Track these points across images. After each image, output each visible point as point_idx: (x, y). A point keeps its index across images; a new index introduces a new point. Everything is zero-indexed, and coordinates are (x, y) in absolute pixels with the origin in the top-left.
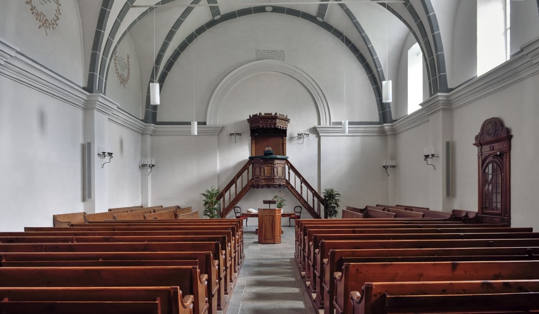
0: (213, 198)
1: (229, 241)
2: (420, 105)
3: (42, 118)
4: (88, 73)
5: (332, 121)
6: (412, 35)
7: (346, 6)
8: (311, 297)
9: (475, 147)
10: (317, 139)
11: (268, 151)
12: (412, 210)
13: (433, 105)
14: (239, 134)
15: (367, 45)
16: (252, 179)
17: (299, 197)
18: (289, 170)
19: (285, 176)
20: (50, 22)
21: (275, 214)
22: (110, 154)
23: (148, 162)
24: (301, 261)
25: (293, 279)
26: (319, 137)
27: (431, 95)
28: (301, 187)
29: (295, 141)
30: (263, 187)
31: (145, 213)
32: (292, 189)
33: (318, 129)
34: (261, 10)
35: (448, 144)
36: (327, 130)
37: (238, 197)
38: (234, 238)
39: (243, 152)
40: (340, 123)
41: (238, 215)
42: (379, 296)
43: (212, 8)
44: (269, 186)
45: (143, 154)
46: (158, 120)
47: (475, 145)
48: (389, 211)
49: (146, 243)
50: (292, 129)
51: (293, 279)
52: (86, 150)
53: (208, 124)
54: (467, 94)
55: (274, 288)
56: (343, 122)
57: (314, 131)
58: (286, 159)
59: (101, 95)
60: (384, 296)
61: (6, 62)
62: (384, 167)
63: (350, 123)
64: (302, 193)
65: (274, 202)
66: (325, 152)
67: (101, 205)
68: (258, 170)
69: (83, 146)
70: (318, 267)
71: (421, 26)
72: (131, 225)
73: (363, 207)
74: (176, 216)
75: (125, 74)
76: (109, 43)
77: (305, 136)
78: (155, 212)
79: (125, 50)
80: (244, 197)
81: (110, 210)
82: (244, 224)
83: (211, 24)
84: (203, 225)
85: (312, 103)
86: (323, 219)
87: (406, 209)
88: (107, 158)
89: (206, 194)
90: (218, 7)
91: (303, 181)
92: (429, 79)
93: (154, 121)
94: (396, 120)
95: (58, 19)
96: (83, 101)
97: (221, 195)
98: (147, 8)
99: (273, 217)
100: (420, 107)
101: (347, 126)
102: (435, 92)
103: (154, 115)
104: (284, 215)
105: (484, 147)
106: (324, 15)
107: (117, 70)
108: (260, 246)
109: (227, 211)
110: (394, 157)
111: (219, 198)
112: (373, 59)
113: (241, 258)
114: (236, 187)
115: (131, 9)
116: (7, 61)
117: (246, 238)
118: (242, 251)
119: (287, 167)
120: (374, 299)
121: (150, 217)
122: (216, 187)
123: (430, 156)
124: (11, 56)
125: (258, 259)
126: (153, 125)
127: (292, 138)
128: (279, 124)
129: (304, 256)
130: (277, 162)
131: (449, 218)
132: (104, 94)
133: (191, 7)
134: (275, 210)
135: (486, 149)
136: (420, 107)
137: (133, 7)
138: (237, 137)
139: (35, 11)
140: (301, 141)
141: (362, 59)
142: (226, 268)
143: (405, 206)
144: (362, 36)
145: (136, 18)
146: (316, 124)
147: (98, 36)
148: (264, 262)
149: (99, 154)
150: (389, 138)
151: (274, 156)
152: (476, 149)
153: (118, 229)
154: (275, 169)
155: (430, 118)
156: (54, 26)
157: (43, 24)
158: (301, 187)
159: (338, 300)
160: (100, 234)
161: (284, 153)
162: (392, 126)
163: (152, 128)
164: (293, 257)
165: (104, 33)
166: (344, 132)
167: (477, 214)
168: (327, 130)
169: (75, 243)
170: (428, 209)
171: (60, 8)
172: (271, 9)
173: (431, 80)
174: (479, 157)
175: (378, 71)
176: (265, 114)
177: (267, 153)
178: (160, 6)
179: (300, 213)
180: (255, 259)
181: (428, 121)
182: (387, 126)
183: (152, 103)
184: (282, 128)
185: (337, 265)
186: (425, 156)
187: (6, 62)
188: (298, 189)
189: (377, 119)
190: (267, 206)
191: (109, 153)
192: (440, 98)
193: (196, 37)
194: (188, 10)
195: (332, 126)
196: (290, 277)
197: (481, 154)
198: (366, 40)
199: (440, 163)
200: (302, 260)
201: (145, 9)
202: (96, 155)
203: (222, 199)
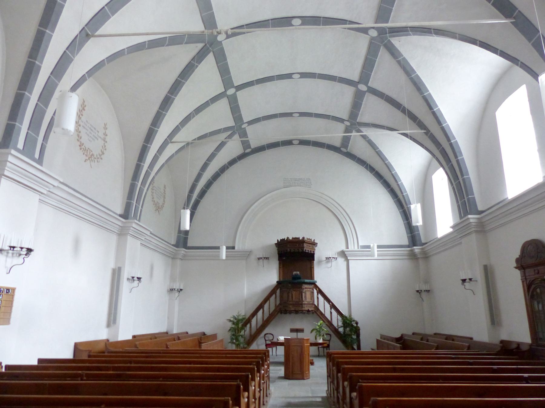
0: (239, 324)
1: (253, 379)
3: (77, 244)
4: (125, 201)
5: (360, 244)
7: (368, 138)
9: (517, 270)
10: (345, 263)
11: (296, 275)
12: (453, 340)
16: (280, 304)
17: (329, 324)
18: (318, 294)
19: (314, 301)
20: (95, 156)
22: (139, 279)
23: (176, 286)
24: (334, 402)
26: (347, 261)
27: (461, 218)
28: (331, 313)
29: (324, 265)
30: (290, 312)
31: (169, 340)
32: (322, 316)
33: (346, 253)
34: (288, 143)
36: (355, 254)
37: (266, 323)
38: (258, 374)
39: (271, 276)
40: (369, 247)
43: (243, 143)
44: (297, 312)
45: (173, 279)
46: (189, 244)
47: (516, 268)
48: (427, 341)
50: (320, 253)
52: (116, 274)
53: (236, 248)
56: (372, 245)
57: (343, 254)
58: (314, 284)
59: (136, 221)
61: (49, 191)
62: (418, 291)
63: (379, 247)
64: (331, 319)
66: (356, 276)
67: (125, 333)
68: (285, 295)
69: (114, 271)
72: (150, 357)
73: (398, 335)
75: (161, 202)
76: (147, 174)
77: (333, 260)
78: (179, 339)
82: (270, 353)
83: (242, 157)
85: (339, 227)
87: (446, 339)
88: (136, 282)
89: (232, 319)
90: (248, 141)
91: (333, 306)
92: (457, 202)
93: (185, 246)
94: (426, 243)
95: (103, 153)
96: (118, 226)
97: (248, 321)
98: (185, 144)
99: (302, 347)
100: (451, 230)
101: (376, 249)
102: (465, 215)
103: (185, 240)
105: (527, 270)
106: (348, 146)
107: (153, 198)
108: (287, 382)
109: (253, 338)
110: (426, 282)
111: (245, 325)
112: (398, 185)
113: (267, 396)
115: (170, 144)
116: (51, 190)
117: (273, 370)
118: (268, 388)
119: (315, 291)
121: (173, 346)
122: (244, 312)
123: (468, 280)
124: (54, 186)
125: (286, 398)
126: (184, 249)
127: (320, 262)
128: (307, 248)
129: (338, 398)
130: (305, 286)
131: (499, 351)
132: (139, 221)
135: (530, 272)
136: (451, 230)
137: (171, 142)
138: (265, 261)
139: (83, 147)
140: (329, 265)
142: (255, 399)
144: (386, 164)
145: (174, 152)
146: (343, 248)
147: (138, 168)
149: (128, 279)
150: (421, 262)
151: (302, 280)
152: (518, 274)
154: (303, 294)
156: (99, 160)
157: (89, 158)
158: (331, 313)
161: (312, 277)
162: (422, 249)
163: (183, 252)
165: (143, 166)
166: (374, 256)
167: (531, 345)
168: (355, 254)
170: (471, 339)
171: (106, 144)
172: (298, 142)
174: (523, 282)
175: (403, 196)
177: (296, 278)
178: (197, 141)
179: (329, 341)
180: (282, 397)
181: (461, 243)
182: (417, 249)
183: (182, 229)
184: (310, 252)
186: (462, 280)
187: (49, 191)
188: (328, 315)
189: (406, 242)
191: (138, 278)
192: (471, 221)
193: (228, 168)
194: (222, 145)
195: (360, 249)
197: (524, 278)
198: (389, 167)
199: (480, 287)
200: (336, 400)
201: (183, 144)
202: (125, 280)
203: (248, 326)
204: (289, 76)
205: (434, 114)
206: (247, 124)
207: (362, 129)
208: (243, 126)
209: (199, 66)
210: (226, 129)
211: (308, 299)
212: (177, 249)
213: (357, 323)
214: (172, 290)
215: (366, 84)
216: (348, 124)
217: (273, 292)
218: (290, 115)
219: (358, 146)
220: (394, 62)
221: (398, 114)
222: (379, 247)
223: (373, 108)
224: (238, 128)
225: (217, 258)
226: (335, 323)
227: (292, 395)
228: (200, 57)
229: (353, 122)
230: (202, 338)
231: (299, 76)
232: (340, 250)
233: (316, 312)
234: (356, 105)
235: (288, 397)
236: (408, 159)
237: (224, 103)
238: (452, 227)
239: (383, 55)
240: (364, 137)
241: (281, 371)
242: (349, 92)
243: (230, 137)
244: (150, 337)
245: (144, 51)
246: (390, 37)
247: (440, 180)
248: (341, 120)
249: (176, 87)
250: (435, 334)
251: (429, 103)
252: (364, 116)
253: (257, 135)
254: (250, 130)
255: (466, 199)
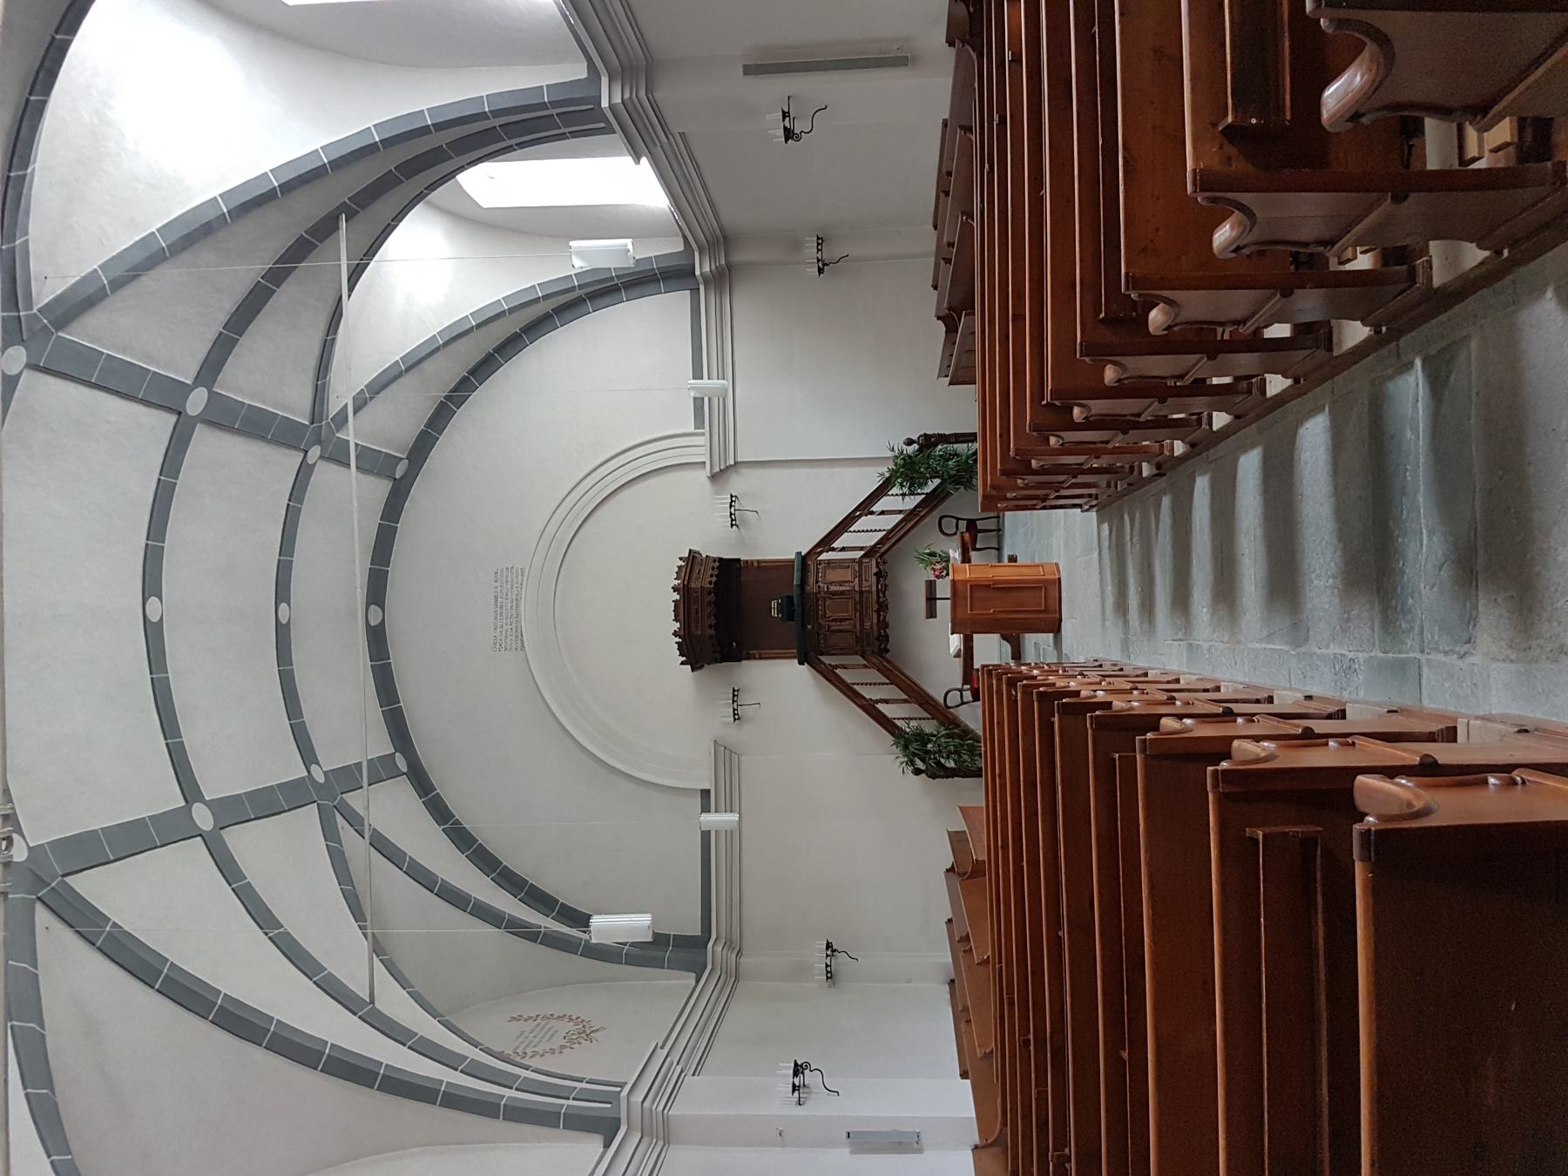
2: (637, 161)
4: (560, 1132)
5: (691, 429)
6: (434, 195)
8: (1226, 432)
10: (745, 471)
13: (636, 118)
14: (735, 694)
15: (471, 330)
17: (912, 518)
18: (834, 549)
21: (966, 581)
22: (798, 1070)
23: (819, 960)
25: (1166, 501)
28: (883, 513)
30: (884, 625)
32: (892, 539)
34: (377, 639)
35: (749, 70)
39: (783, 684)
40: (699, 403)
41: (968, 696)
42: (1232, 150)
44: (883, 607)
48: (949, 174)
49: (1065, 934)
50: (717, 543)
51: (1166, 501)
53: (706, 786)
54: (604, 17)
55: (1194, 555)
58: (804, 560)
60: (1230, 133)
62: (821, 271)
64: (900, 512)
65: (931, 586)
70: (1127, 406)
71: (412, 168)
74: (978, 870)
78: (966, 939)
79: (497, 1029)
80: (914, 678)
81: (964, 1075)
83: (422, 783)
84: (1002, 775)
86: (977, 446)
87: (947, 194)
88: (809, 1077)
91: (865, 507)
92: (562, 137)
99: (977, 586)
100: (644, 160)
103: (683, 942)
104: (966, 559)
107: (553, 1051)
114: (886, 701)
118: (1075, 665)
119: (824, 556)
120: (1240, 166)
128: (705, 580)
130: (811, 586)
132: (622, 1085)
133: (371, 837)
134: (954, 582)
136: (644, 160)
137: (372, 1002)
141: (511, 346)
143: (938, 197)
148: (1110, 600)
150: (736, 258)
151: (795, 593)
153: (1025, 1030)
154: (833, 588)
155: (676, 130)
158: (883, 513)
159: (1237, 314)
160: (1042, 1082)
163: (719, 948)
164: (1093, 514)
169: (1072, 1150)
170: (945, 124)
173: (563, 130)
175: (545, 297)
176: (676, 620)
179: (958, 519)
181: (682, 135)
182: (702, 267)
184: (716, 572)
185: (1121, 327)
188: (891, 521)
189: (678, 301)
190: (944, 608)
191: (796, 1074)
192: (617, 100)
194: (381, 844)
196: (1159, 506)
202: (800, 1111)
204: (153, 633)
205: (288, 187)
206: (314, 767)
207: (333, 408)
208: (321, 779)
209: (114, 919)
210: (330, 833)
211: (847, 575)
212: (709, 967)
213: (910, 442)
214: (830, 975)
215: (184, 390)
216: (315, 452)
217: (830, 675)
218: (283, 632)
219: (390, 424)
220: (114, 302)
221: (286, 294)
222: (697, 374)
223: (268, 374)
224: (327, 796)
225: (733, 836)
226: (911, 502)
227: (1096, 605)
228: (85, 921)
229: (311, 436)
230: (964, 873)
231: (153, 600)
232: (708, 482)
233: (882, 552)
234: (256, 425)
235: (1103, 613)
236: (423, 279)
237: (244, 841)
238: (637, 160)
239: (86, 333)
240: (360, 403)
241: (1037, 645)
242: (207, 444)
243: (355, 821)
244: (963, 1026)
245: (59, 1100)
246: (29, 306)
247: (492, 183)
248: (303, 474)
249: (187, 993)
250: (936, 227)
251: (254, 203)
252: (294, 403)
253: (349, 730)
254: (332, 757)
255: (554, 112)
